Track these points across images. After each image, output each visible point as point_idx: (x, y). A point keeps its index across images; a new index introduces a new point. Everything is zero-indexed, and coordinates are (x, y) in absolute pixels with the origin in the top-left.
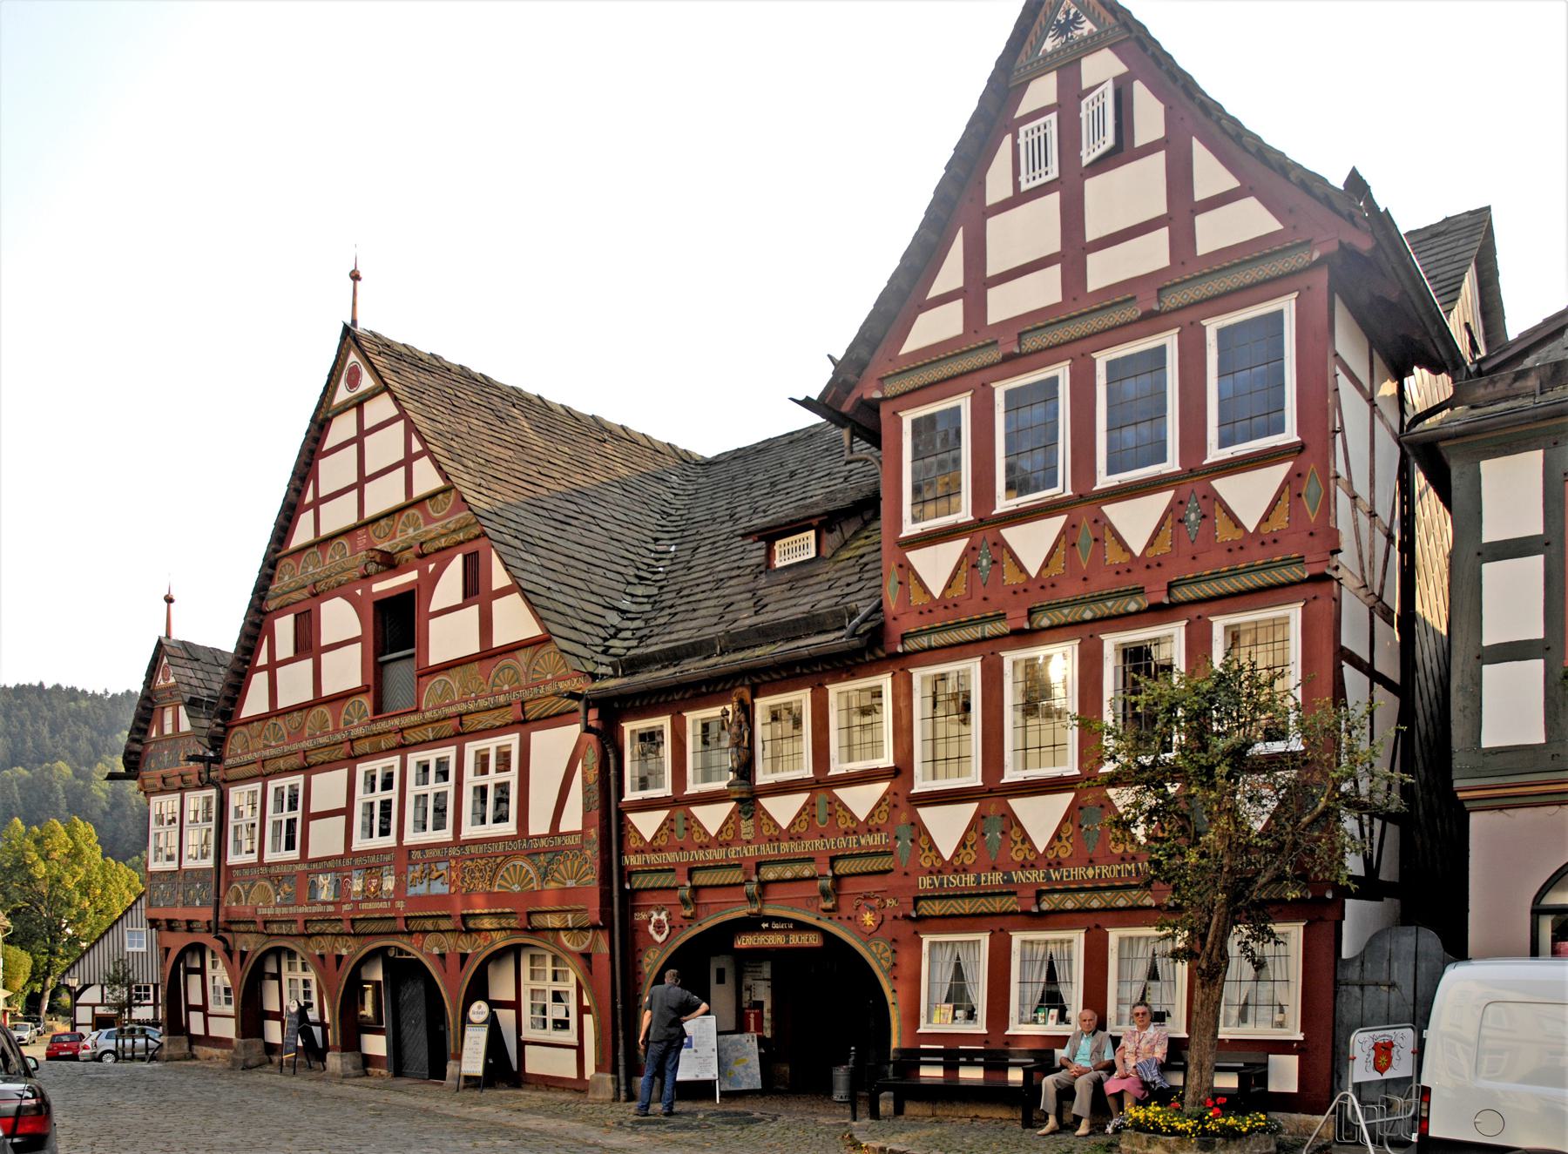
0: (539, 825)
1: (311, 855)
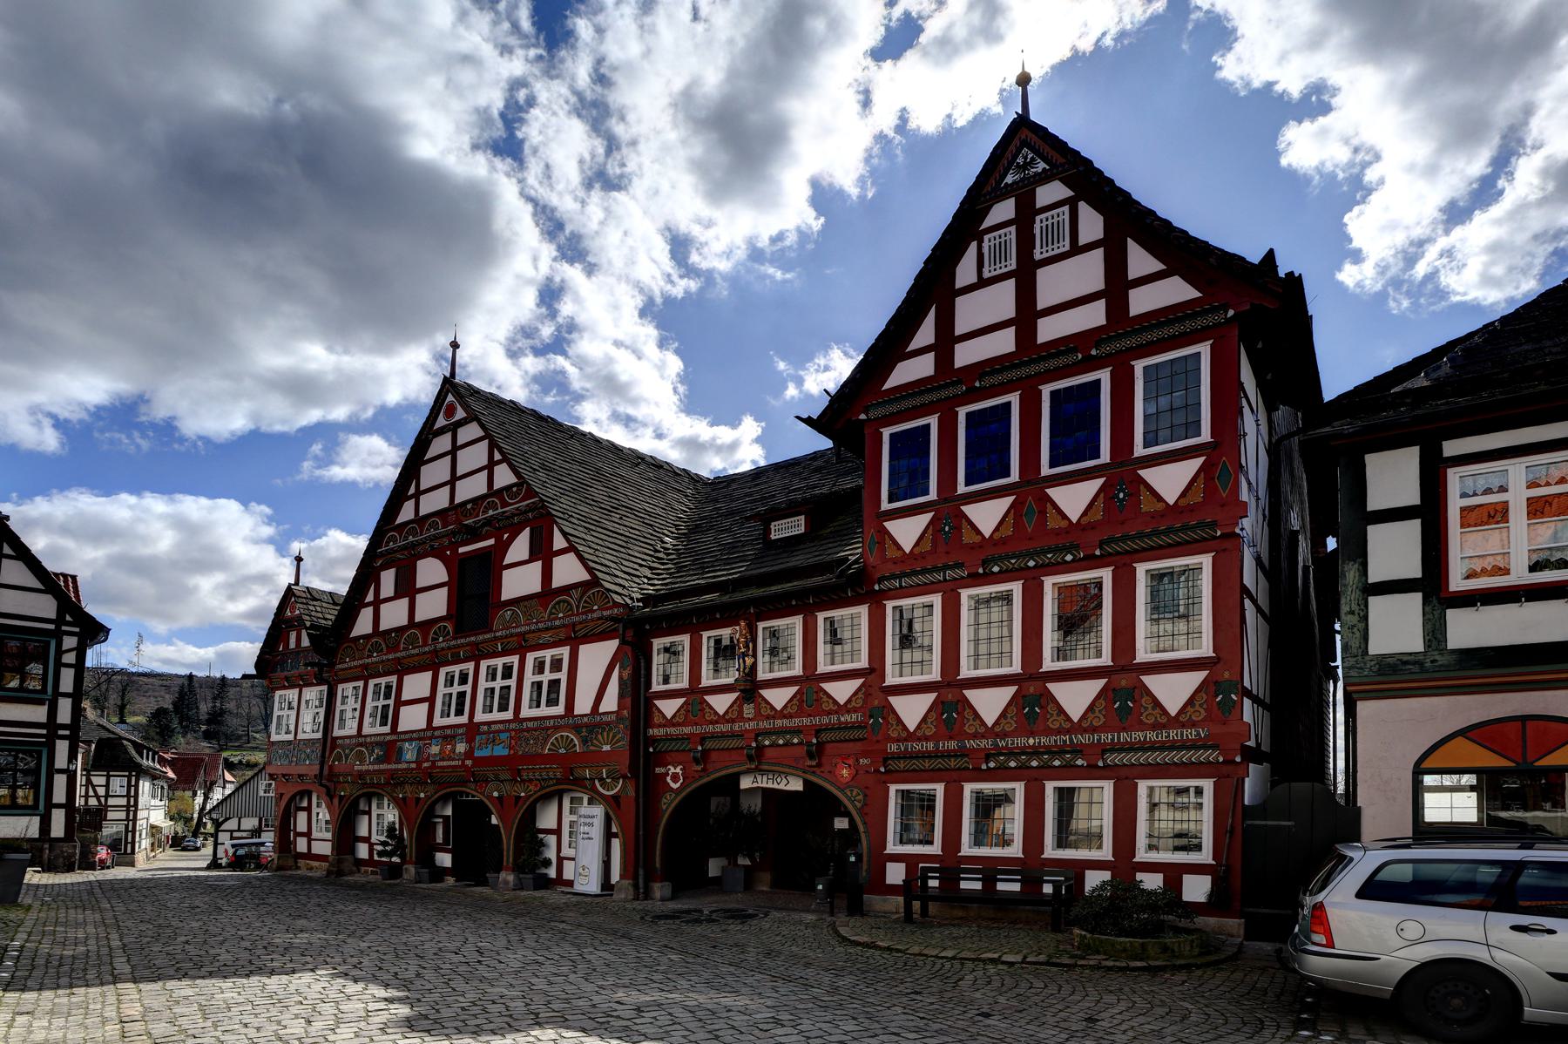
0: (583, 706)
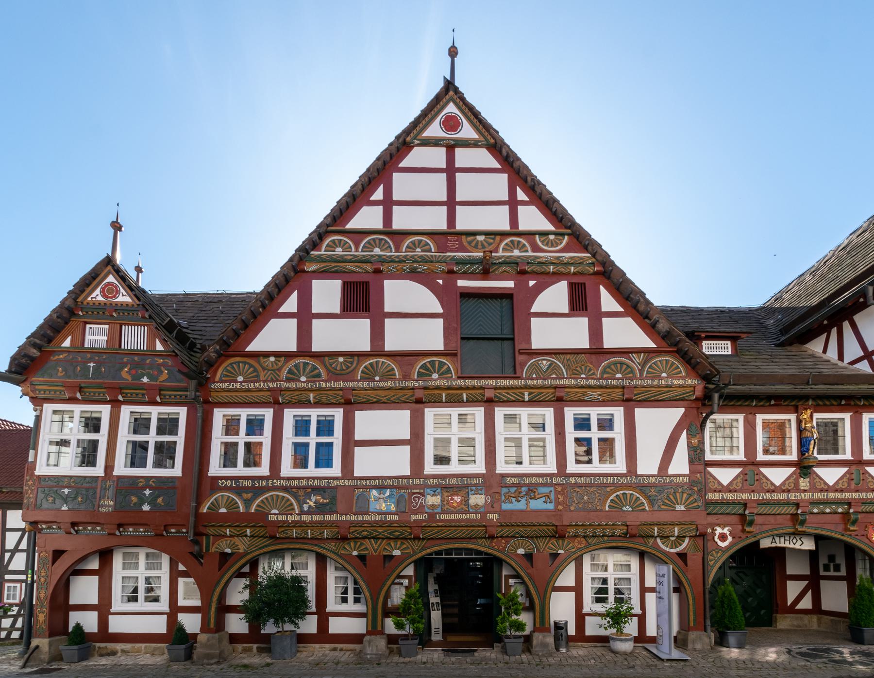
0: (648, 465)
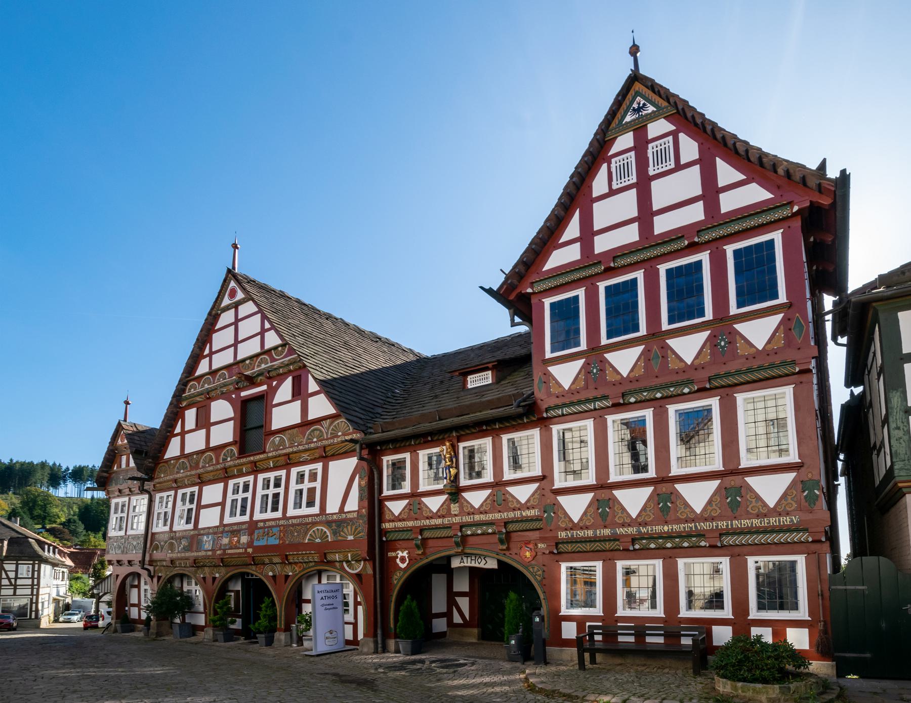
0: (333, 507)
1: (200, 526)
